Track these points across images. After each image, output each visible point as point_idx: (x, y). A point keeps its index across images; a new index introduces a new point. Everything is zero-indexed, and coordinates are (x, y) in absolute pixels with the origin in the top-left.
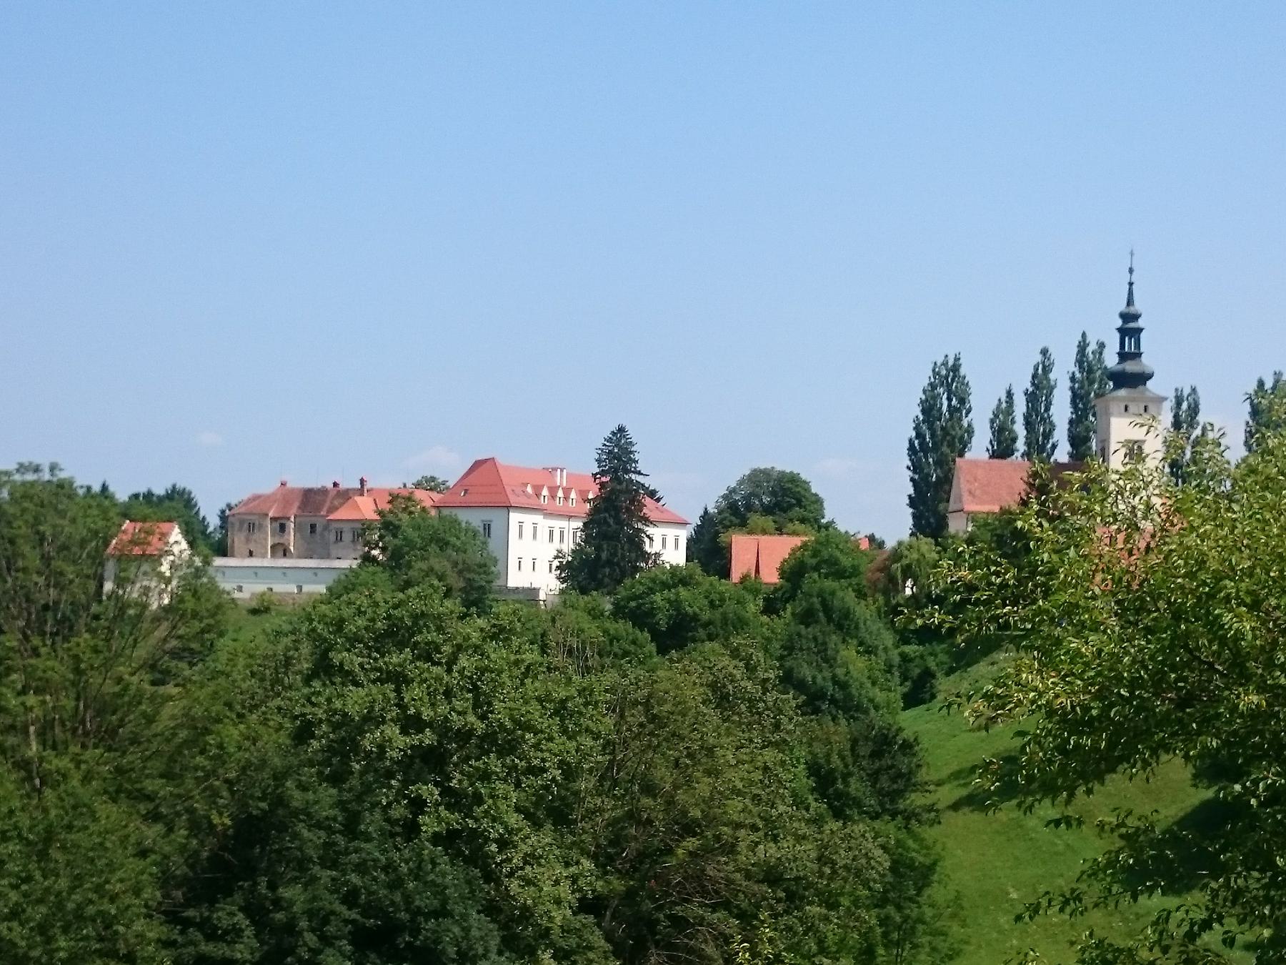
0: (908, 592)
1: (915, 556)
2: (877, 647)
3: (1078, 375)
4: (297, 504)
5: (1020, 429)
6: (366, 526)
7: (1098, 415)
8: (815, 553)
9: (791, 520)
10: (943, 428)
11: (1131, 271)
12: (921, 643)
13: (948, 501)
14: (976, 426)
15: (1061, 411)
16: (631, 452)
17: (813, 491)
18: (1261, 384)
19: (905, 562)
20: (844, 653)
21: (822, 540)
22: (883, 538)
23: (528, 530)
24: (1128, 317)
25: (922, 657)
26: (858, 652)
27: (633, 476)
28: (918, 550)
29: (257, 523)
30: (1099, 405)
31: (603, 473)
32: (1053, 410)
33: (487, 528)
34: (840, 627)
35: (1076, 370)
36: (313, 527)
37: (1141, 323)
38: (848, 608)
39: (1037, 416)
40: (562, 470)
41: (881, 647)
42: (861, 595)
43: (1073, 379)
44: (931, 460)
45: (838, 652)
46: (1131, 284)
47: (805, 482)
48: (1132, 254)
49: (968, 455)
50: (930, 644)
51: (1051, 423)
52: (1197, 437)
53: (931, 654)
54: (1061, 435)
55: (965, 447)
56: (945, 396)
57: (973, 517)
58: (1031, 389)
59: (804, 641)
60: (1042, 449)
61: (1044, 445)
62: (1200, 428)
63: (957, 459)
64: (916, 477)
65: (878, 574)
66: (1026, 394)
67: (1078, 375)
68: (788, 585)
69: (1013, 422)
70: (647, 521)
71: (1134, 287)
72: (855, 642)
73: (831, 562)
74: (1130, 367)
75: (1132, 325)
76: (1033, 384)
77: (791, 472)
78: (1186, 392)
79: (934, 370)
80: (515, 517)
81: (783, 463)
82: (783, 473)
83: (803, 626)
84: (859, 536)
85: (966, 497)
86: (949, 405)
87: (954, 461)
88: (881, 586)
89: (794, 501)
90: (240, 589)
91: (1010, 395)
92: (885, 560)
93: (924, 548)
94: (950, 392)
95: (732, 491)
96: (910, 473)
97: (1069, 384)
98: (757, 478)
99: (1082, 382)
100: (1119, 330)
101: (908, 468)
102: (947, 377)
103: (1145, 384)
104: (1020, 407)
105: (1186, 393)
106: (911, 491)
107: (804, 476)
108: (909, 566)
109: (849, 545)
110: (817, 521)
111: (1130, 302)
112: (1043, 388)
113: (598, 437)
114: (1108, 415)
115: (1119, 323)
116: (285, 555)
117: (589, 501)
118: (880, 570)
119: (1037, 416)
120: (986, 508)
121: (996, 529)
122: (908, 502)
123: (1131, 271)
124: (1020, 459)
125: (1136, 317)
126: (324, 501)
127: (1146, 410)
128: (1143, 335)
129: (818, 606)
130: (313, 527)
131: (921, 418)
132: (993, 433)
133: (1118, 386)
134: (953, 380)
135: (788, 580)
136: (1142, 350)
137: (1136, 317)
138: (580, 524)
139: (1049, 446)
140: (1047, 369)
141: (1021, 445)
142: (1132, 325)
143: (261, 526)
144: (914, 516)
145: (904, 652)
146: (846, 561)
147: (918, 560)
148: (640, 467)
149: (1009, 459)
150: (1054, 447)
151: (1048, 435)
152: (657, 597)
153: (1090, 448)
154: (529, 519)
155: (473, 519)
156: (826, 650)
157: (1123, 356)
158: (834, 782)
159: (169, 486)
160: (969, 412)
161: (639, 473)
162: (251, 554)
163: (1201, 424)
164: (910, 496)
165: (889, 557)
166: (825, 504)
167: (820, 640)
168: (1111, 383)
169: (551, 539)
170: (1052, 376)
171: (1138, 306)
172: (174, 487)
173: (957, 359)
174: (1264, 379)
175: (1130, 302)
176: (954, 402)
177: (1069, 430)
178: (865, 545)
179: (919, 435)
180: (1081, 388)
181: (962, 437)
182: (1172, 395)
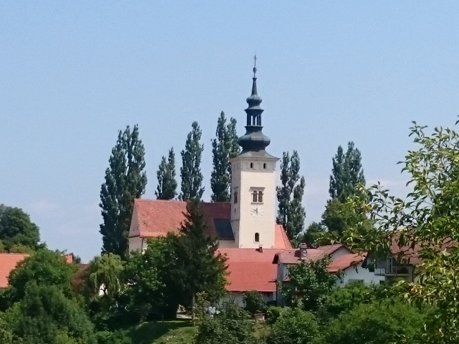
0: (101, 293)
1: (107, 267)
2: (82, 332)
3: (218, 142)
5: (178, 179)
7: (232, 170)
8: (34, 268)
9: (16, 243)
10: (125, 178)
11: (255, 70)
12: (111, 329)
13: (128, 229)
14: (148, 177)
17: (32, 222)
18: (340, 150)
19: (99, 271)
20: (60, 336)
21: (39, 257)
22: (80, 256)
24: (253, 102)
25: (112, 339)
26: (69, 336)
28: (109, 263)
30: (234, 162)
32: (201, 166)
34: (56, 317)
35: (217, 138)
37: (261, 106)
38: (62, 303)
39: (190, 171)
41: (85, 332)
42: (68, 295)
43: (214, 144)
44: (117, 200)
45: (55, 335)
46: (254, 79)
47: (26, 215)
48: (255, 58)
49: (143, 197)
50: (118, 330)
51: (200, 175)
52: (298, 186)
53: (119, 337)
55: (141, 191)
56: (127, 155)
57: (149, 240)
58: (186, 151)
59: (31, 328)
60: (193, 193)
61: (195, 191)
62: (299, 180)
63: (135, 199)
64: (106, 212)
65: (81, 281)
66: (182, 154)
67: (218, 142)
68: (15, 289)
69: (174, 174)
71: (257, 81)
72: (67, 328)
73: (46, 273)
74: (254, 136)
75: (255, 108)
76: (187, 147)
77: (16, 208)
78: (291, 155)
79: (119, 137)
82: (10, 210)
83: (30, 317)
84: (66, 253)
85: (142, 226)
86: (130, 161)
87: (133, 201)
88: (82, 289)
89: (17, 229)
91: (171, 154)
92: (86, 270)
93: (114, 262)
94: (130, 152)
96: (101, 209)
97: (212, 148)
99: (220, 146)
100: (247, 111)
101: (101, 206)
102: (128, 142)
103: (264, 149)
104: (179, 163)
105: (290, 156)
106: (102, 222)
107: (25, 211)
108: (102, 275)
109: (59, 260)
110: (34, 243)
111: (254, 92)
112: (194, 151)
113: (409, 137)
114: (239, 169)
115: (247, 106)
118: (82, 277)
119: (190, 171)
120: (155, 234)
121: (164, 248)
122: (100, 229)
123: (255, 70)
124: (178, 200)
125: (258, 102)
127: (264, 167)
128: (263, 115)
129: (40, 303)
131: (111, 169)
132: (160, 182)
133: (245, 150)
134: (133, 144)
135: (14, 285)
136: (262, 125)
137: (258, 102)
139: (198, 191)
141: (179, 190)
142: (255, 108)
144: (104, 239)
145: (99, 336)
146: (56, 272)
147: (109, 271)
149: (171, 200)
150: (202, 191)
151: (197, 183)
153: (226, 193)
156: (46, 334)
157: (250, 129)
160: (143, 166)
163: (301, 177)
164: (101, 226)
165: (89, 268)
166: (40, 232)
167: (43, 327)
168: (241, 148)
170: (200, 142)
171: (260, 95)
173: (136, 129)
174: (342, 146)
175: (254, 92)
176: (133, 159)
177: (212, 180)
178: (70, 261)
179: (108, 181)
180: (221, 150)
181: (139, 184)
182: (281, 156)
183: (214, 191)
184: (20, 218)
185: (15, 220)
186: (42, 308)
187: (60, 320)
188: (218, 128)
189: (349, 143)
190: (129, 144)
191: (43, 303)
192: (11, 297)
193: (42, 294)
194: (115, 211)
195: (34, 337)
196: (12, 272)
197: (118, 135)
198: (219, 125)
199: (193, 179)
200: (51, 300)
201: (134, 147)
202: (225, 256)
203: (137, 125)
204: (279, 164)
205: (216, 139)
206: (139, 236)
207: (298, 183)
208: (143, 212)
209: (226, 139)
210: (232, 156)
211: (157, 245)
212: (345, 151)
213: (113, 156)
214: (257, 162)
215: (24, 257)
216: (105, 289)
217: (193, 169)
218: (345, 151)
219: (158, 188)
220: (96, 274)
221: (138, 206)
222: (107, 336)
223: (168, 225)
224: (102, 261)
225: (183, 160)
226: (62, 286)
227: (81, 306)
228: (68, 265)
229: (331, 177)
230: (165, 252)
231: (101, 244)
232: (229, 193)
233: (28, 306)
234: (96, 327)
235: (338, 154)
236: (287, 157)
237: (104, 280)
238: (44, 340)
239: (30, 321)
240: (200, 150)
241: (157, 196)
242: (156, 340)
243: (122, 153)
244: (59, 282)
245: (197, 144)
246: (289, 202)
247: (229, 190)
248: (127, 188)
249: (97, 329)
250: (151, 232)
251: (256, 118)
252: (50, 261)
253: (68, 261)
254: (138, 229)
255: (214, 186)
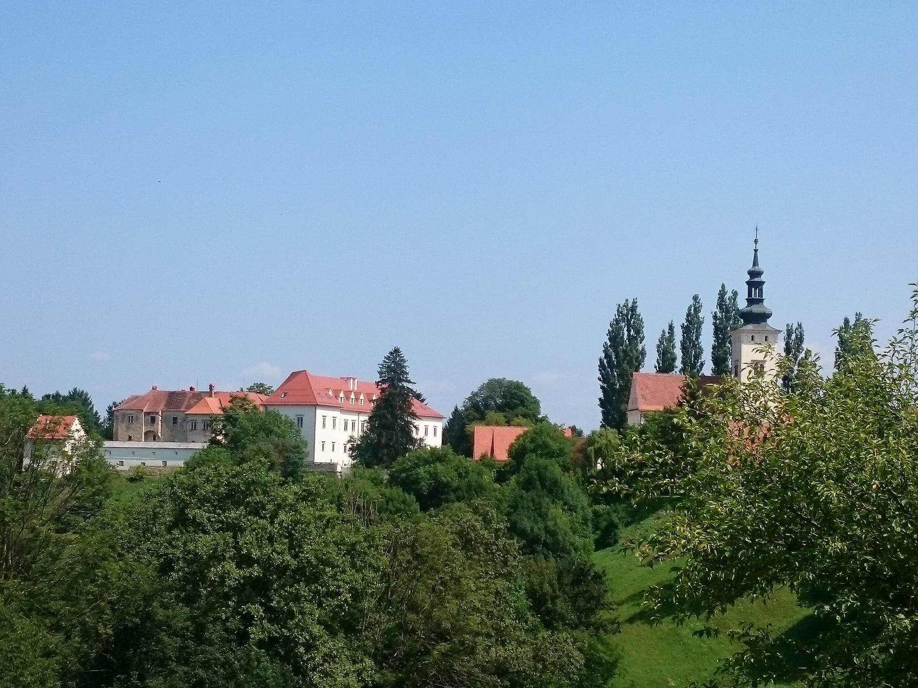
0: (599, 467)
1: (604, 442)
2: (576, 507)
3: (719, 315)
4: (164, 403)
5: (678, 352)
6: (213, 419)
8: (533, 441)
9: (517, 416)
11: (756, 241)
12: (608, 503)
15: (707, 340)
16: (404, 367)
18: (847, 321)
19: (597, 445)
23: (329, 422)
24: (753, 274)
25: (608, 514)
26: (563, 510)
27: (405, 384)
29: (134, 416)
30: (734, 335)
31: (383, 381)
32: (701, 339)
33: (300, 420)
34: (550, 492)
35: (718, 310)
36: (175, 419)
37: (763, 278)
39: (690, 343)
40: (354, 379)
42: (565, 469)
43: (715, 317)
46: (756, 251)
49: (642, 370)
51: (700, 348)
53: (615, 511)
54: (707, 357)
55: (640, 364)
56: (626, 329)
57: (645, 414)
58: (686, 324)
60: (693, 366)
61: (695, 364)
62: (804, 352)
65: (578, 454)
66: (682, 327)
68: (514, 462)
69: (674, 347)
70: (414, 415)
72: (561, 503)
73: (545, 446)
74: (755, 309)
75: (756, 279)
76: (687, 320)
79: (618, 310)
80: (320, 413)
81: (511, 375)
82: (511, 383)
85: (640, 400)
86: (629, 335)
87: (632, 375)
88: (580, 462)
89: (518, 402)
90: (122, 463)
91: (671, 328)
93: (611, 436)
94: (629, 325)
95: (475, 395)
97: (712, 321)
98: (493, 386)
101: (599, 379)
103: (766, 321)
107: (526, 385)
110: (535, 416)
111: (755, 263)
114: (740, 342)
115: (748, 278)
116: (154, 439)
117: (372, 401)
118: (580, 451)
120: (654, 408)
123: (756, 241)
125: (759, 274)
126: (184, 400)
127: (752, 340)
128: (764, 287)
130: (175, 419)
131: (609, 344)
133: (747, 322)
134: (631, 317)
137: (759, 274)
138: (367, 418)
140: (697, 310)
141: (679, 364)
142: (756, 279)
143: (137, 418)
144: (603, 413)
146: (554, 446)
147: (606, 445)
148: (410, 377)
149: (671, 373)
150: (702, 365)
151: (698, 356)
152: (421, 470)
153: (727, 366)
154: (330, 414)
155: (289, 413)
156: (540, 508)
157: (751, 301)
158: (546, 601)
159: (72, 390)
161: (409, 382)
162: (130, 439)
163: (805, 349)
164: (600, 399)
165: (586, 442)
167: (537, 502)
169: (346, 428)
170: (701, 315)
171: (761, 266)
172: (75, 390)
173: (634, 302)
175: (755, 263)
176: (632, 333)
178: (568, 434)
179: (607, 356)
181: (638, 357)
183: (714, 364)
184: (521, 391)
185: (516, 393)
186: (538, 483)
187: (554, 494)
188: (718, 300)
189: (857, 315)
190: (628, 318)
191: (539, 477)
192: (510, 469)
193: (537, 468)
194: (615, 384)
195: (528, 511)
196: (511, 446)
197: (617, 308)
198: (719, 298)
199: (693, 353)
200: (546, 475)
201: (633, 320)
202: (396, 467)
203: (636, 299)
204: (782, 336)
205: (716, 312)
206: (637, 409)
207: (802, 355)
208: (641, 386)
209: (727, 311)
210: (733, 329)
211: (654, 419)
212: (852, 322)
213: (611, 329)
214: (759, 334)
215: (523, 430)
216: (602, 463)
217: (694, 342)
218: (852, 322)
219: (658, 362)
220: (593, 448)
221: (636, 379)
222: (603, 510)
223: (667, 398)
224: (599, 435)
225: (684, 333)
226: (560, 459)
227: (578, 481)
228: (567, 439)
229: (837, 349)
230: (661, 427)
231: (600, 417)
232: (730, 366)
233: (524, 480)
234: (593, 501)
235: (840, 360)
236: (791, 329)
237: (601, 454)
238: (538, 514)
239: (525, 496)
240: (700, 323)
241: (656, 370)
242: (653, 515)
243: (621, 327)
244: (558, 455)
245: (698, 318)
246: (793, 374)
247: (730, 363)
248: (626, 362)
249: (594, 503)
250: (650, 405)
251: (757, 290)
252: (548, 435)
253: (566, 435)
254: (636, 403)
255: (714, 359)
